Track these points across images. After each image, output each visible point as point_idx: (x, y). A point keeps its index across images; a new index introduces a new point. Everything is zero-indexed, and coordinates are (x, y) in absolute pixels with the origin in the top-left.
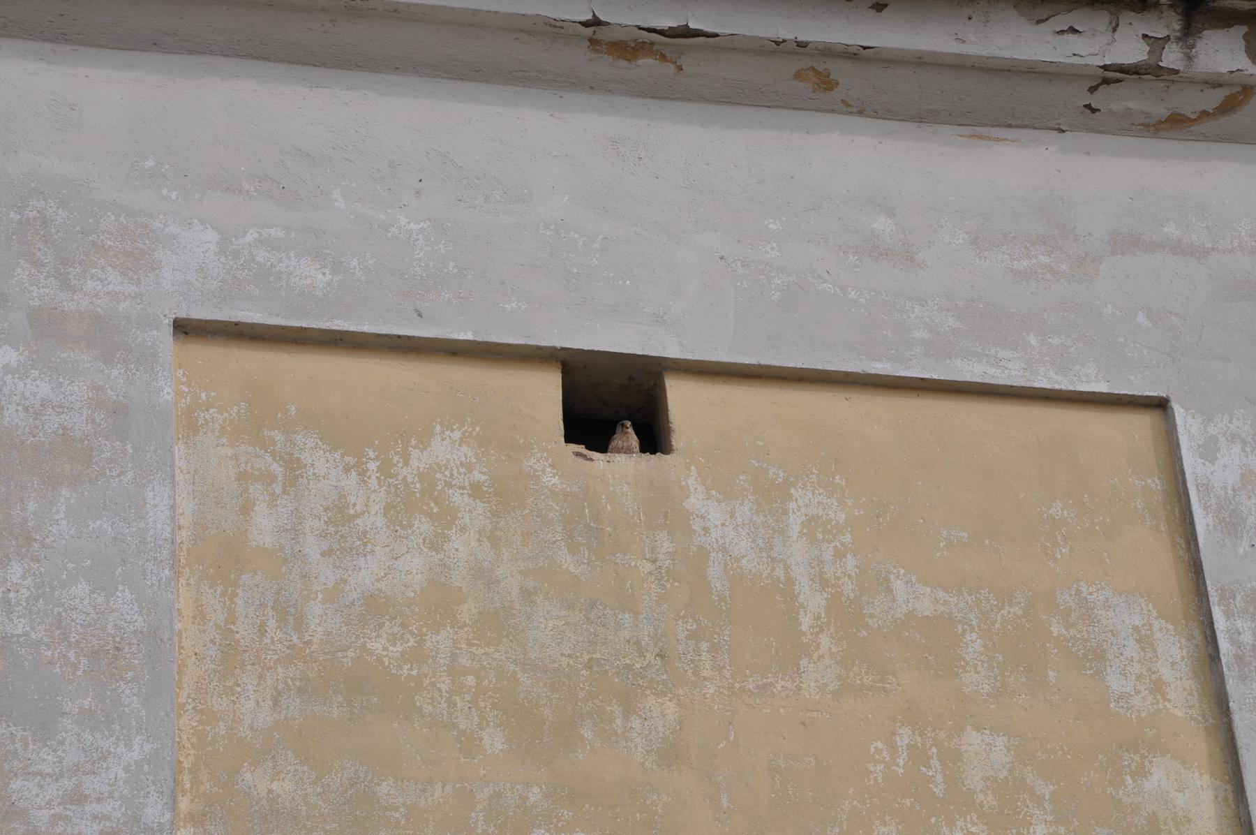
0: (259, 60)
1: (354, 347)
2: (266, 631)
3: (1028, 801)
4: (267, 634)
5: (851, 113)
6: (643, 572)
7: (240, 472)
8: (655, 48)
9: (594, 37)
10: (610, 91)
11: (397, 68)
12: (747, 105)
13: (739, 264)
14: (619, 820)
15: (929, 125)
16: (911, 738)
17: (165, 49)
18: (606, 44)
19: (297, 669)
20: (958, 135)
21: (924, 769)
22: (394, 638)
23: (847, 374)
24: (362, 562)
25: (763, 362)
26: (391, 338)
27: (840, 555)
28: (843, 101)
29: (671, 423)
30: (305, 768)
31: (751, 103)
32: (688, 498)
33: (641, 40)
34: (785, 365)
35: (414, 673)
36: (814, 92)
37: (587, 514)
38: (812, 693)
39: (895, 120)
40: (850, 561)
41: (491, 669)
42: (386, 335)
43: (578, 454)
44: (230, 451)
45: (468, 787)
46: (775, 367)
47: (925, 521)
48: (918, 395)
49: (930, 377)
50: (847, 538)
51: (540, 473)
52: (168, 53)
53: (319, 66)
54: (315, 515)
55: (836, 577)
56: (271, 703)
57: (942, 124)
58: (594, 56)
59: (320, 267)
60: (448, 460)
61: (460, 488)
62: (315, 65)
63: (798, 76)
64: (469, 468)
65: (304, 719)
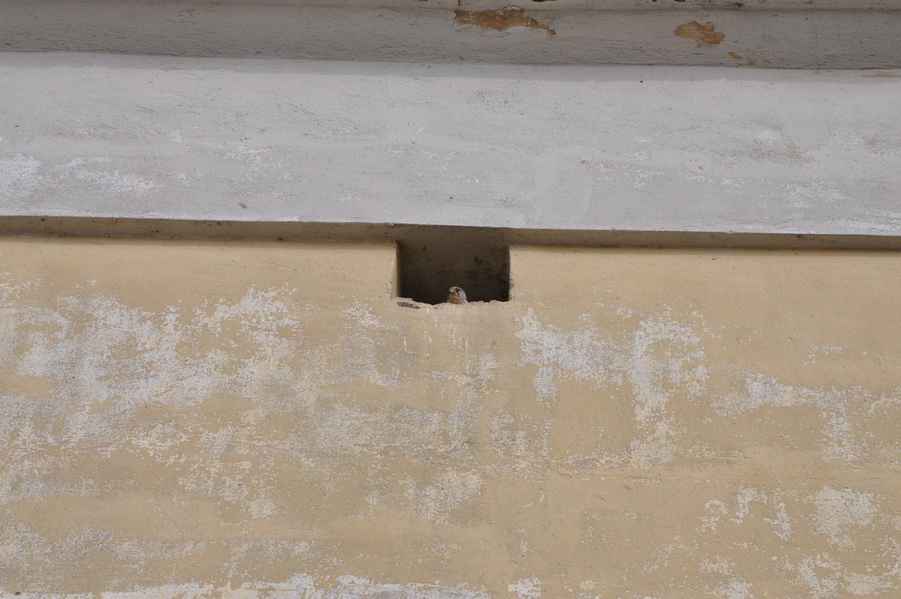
0: (116, 53)
1: (172, 238)
2: (19, 435)
3: (894, 543)
4: (19, 438)
5: (740, 65)
6: (461, 384)
7: (22, 325)
8: (525, 14)
9: (461, 8)
10: (481, 60)
11: (258, 52)
12: (628, 64)
13: (602, 166)
14: (397, 565)
15: (828, 70)
16: (755, 496)
17: (18, 48)
18: (473, 15)
19: (47, 461)
20: (861, 76)
21: (768, 520)
22: (164, 437)
23: (713, 235)
24: (142, 383)
25: (617, 228)
26: (211, 225)
27: (689, 367)
28: (731, 54)
29: (512, 280)
30: (37, 535)
31: (632, 62)
32: (521, 329)
33: (510, 9)
34: (642, 230)
35: (182, 460)
36: (699, 46)
37: (405, 345)
38: (641, 465)
39: (791, 68)
40: (701, 371)
41: (271, 456)
42: (205, 222)
44: (14, 311)
45: (225, 544)
46: (631, 232)
47: (792, 341)
48: (796, 254)
49: (808, 233)
50: (701, 354)
51: (358, 318)
52: (21, 51)
53: (179, 56)
54: (98, 353)
55: (682, 382)
56: (9, 488)
57: (843, 69)
58: (459, 27)
59: (144, 179)
60: (257, 312)
61: (265, 330)
62: (174, 55)
63: (679, 32)
64: (279, 316)
65: (44, 498)
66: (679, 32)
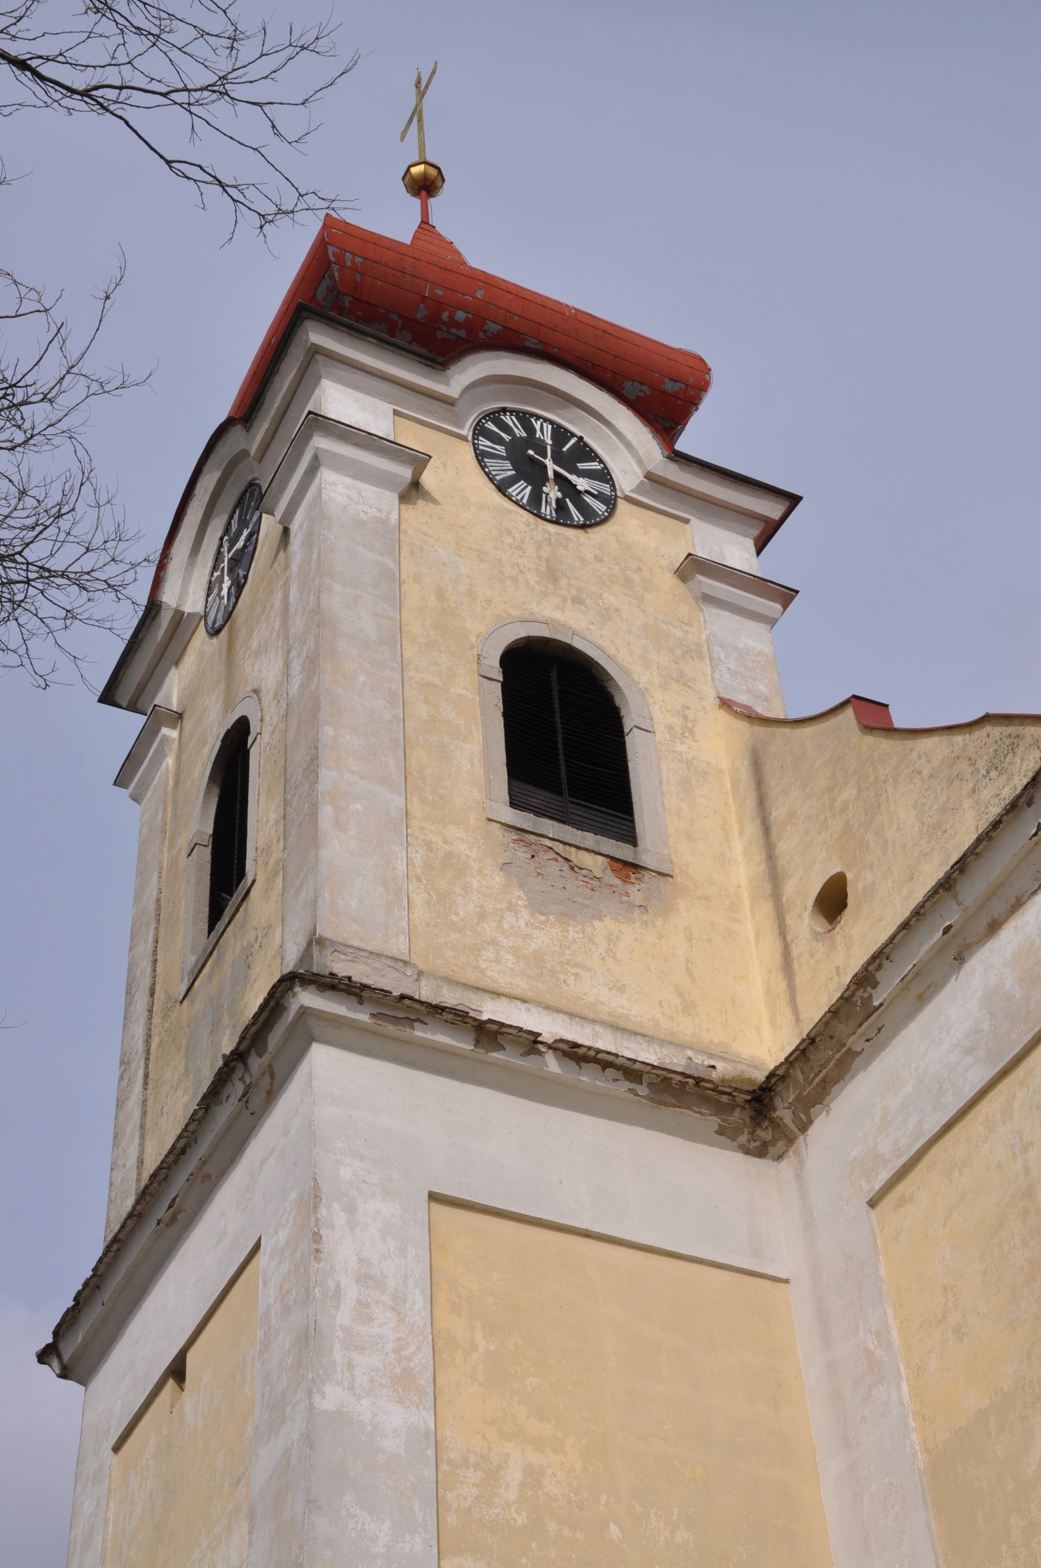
43: (630, 1090)
63: (203, 1182)
66: (203, 1182)
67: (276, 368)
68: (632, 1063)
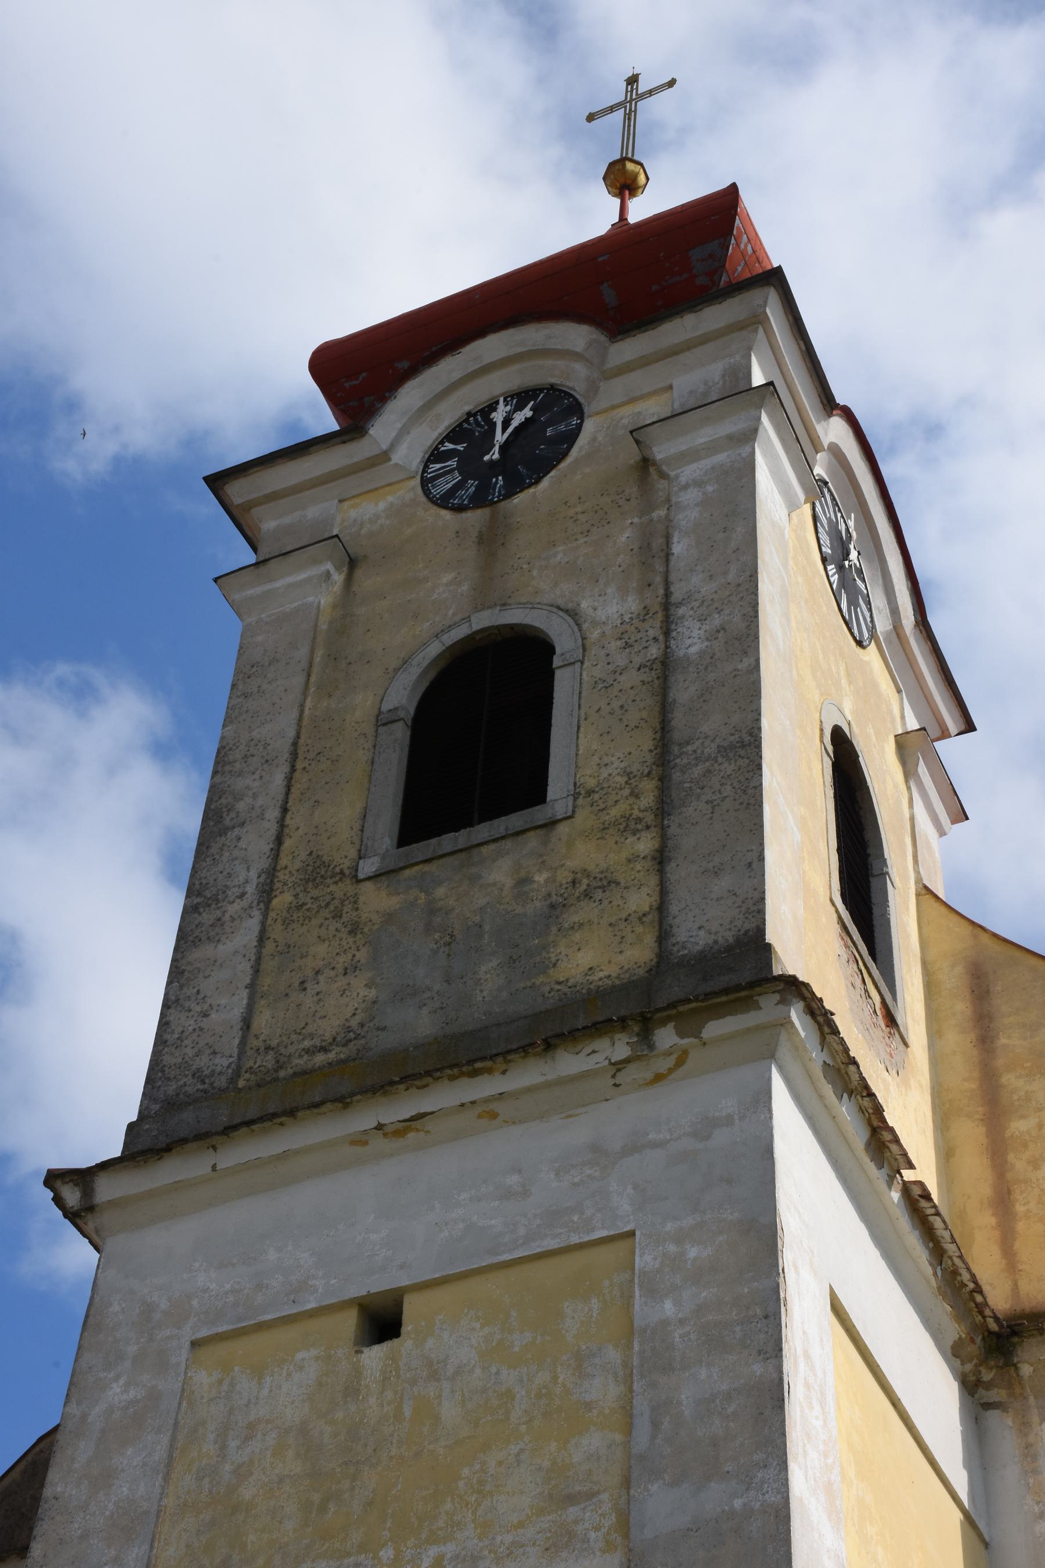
63: (479, 1116)
67: (699, 307)
68: (950, 1241)
